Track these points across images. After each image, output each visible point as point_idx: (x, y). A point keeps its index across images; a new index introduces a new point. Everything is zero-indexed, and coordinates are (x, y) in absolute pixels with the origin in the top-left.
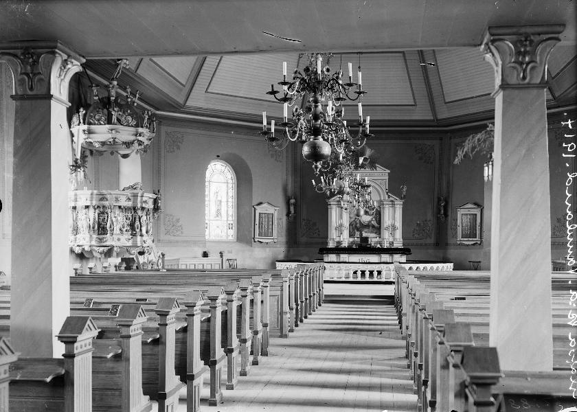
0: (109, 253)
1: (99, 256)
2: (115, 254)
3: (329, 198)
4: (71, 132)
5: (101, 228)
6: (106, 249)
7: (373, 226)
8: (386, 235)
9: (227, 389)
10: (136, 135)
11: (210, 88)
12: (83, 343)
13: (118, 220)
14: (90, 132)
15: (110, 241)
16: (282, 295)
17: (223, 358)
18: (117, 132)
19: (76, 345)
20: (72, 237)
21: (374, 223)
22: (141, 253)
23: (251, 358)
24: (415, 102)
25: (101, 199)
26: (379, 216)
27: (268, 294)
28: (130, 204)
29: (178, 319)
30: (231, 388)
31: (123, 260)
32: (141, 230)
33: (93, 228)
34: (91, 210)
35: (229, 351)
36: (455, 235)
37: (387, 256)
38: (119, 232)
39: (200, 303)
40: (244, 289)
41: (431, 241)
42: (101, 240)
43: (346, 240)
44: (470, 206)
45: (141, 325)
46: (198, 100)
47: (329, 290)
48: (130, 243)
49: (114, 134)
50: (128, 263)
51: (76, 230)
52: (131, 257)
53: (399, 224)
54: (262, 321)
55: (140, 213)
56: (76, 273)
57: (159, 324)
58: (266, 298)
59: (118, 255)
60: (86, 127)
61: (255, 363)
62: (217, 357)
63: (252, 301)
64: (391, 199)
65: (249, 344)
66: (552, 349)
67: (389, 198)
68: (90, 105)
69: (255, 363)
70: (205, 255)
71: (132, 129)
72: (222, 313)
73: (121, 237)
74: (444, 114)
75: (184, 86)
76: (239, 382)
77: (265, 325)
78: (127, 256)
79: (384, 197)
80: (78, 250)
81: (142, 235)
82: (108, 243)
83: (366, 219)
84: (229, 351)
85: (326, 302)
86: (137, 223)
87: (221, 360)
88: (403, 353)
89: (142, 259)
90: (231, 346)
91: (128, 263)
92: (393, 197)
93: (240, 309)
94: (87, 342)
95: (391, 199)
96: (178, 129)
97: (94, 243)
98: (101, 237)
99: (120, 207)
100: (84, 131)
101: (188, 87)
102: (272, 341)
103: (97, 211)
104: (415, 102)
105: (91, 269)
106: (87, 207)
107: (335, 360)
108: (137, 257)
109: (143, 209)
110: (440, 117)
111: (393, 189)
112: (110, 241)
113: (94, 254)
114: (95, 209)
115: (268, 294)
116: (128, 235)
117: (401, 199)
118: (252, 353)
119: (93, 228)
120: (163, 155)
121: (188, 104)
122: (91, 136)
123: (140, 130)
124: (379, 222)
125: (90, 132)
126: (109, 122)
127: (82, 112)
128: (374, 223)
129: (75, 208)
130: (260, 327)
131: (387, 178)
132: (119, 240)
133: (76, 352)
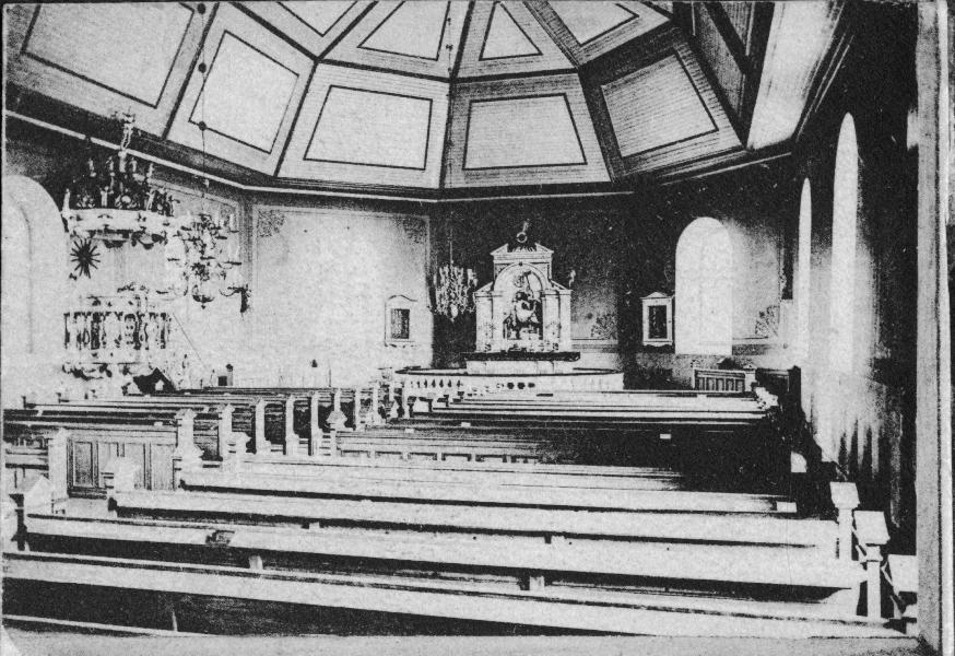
7: (533, 324)
8: (549, 334)
9: (322, 526)
13: (112, 327)
21: (535, 320)
24: (585, 159)
26: (539, 309)
28: (131, 310)
37: (548, 363)
43: (501, 344)
44: (657, 294)
46: (293, 169)
49: (106, 220)
64: (555, 288)
66: (176, 632)
67: (553, 285)
74: (182, 134)
79: (546, 284)
83: (524, 315)
92: (557, 286)
95: (555, 288)
98: (94, 351)
104: (585, 159)
110: (171, 137)
111: (559, 275)
112: (103, 356)
117: (568, 287)
120: (254, 239)
124: (540, 317)
126: (98, 205)
128: (535, 320)
131: (550, 260)
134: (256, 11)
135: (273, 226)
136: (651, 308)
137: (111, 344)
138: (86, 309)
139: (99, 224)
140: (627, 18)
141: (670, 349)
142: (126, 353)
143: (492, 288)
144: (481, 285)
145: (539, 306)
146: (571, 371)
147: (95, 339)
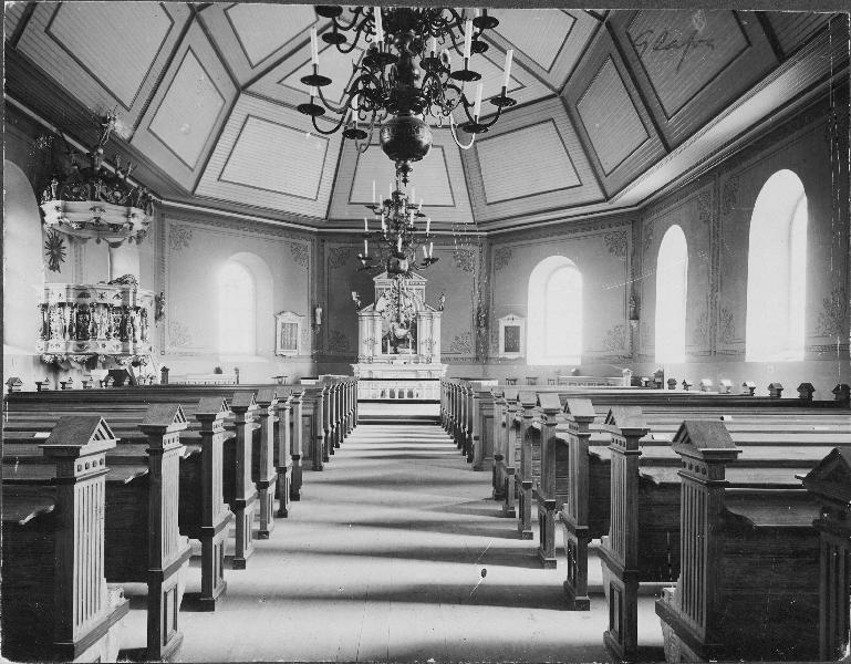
0: (91, 362)
1: (78, 367)
2: (99, 364)
3: (359, 309)
4: (41, 210)
5: (80, 331)
6: (86, 358)
10: (127, 216)
11: (224, 174)
12: (89, 460)
13: (103, 320)
14: (65, 210)
15: (92, 347)
16: (315, 415)
17: (228, 520)
18: (101, 210)
19: (77, 462)
20: (43, 344)
22: (136, 364)
23: (276, 506)
25: (82, 296)
26: (413, 328)
27: (300, 413)
28: (118, 303)
29: (184, 441)
30: (239, 564)
31: (111, 373)
32: (134, 335)
33: (70, 330)
34: (68, 310)
35: (238, 507)
36: (496, 349)
38: (104, 337)
39: (253, 407)
40: (264, 405)
41: (472, 354)
42: (81, 346)
45: (178, 434)
46: (209, 187)
47: (363, 410)
48: (119, 352)
50: (118, 376)
51: (47, 332)
52: (122, 368)
53: (437, 338)
54: (291, 452)
55: (133, 313)
56: (39, 389)
57: (147, 451)
58: (297, 418)
59: (104, 367)
60: (59, 203)
61: (282, 514)
62: (216, 521)
63: (276, 425)
65: (271, 490)
68: (66, 177)
69: (282, 514)
70: (218, 371)
71: (124, 209)
72: (225, 444)
73: (106, 342)
75: (192, 170)
76: (257, 551)
77: (295, 458)
78: (116, 367)
80: (48, 359)
81: (135, 342)
82: (89, 351)
83: (401, 332)
84: (238, 507)
85: (360, 423)
86: (129, 325)
87: (223, 525)
88: (489, 491)
89: (136, 371)
90: (243, 497)
91: (118, 376)
93: (258, 437)
94: (97, 458)
96: (188, 223)
97: (70, 350)
98: (80, 343)
99: (105, 305)
100: (57, 208)
101: (197, 172)
102: (306, 476)
103: (76, 310)
105: (63, 384)
106: (62, 305)
107: (408, 505)
108: (130, 368)
109: (137, 309)
112: (92, 347)
113: (73, 364)
114: (73, 308)
115: (300, 413)
116: (116, 342)
118: (277, 496)
119: (70, 330)
121: (198, 192)
122: (68, 214)
123: (133, 210)
125: (65, 210)
127: (55, 184)
129: (45, 306)
130: (289, 462)
132: (104, 346)
133: (76, 474)
134: (798, 210)
135: (182, 239)
136: (506, 328)
137: (101, 335)
138: (72, 299)
139: (89, 216)
140: (200, 31)
141: (522, 360)
142: (113, 346)
143: (374, 308)
144: (363, 306)
145: (414, 326)
146: (202, 399)
147: (80, 331)
